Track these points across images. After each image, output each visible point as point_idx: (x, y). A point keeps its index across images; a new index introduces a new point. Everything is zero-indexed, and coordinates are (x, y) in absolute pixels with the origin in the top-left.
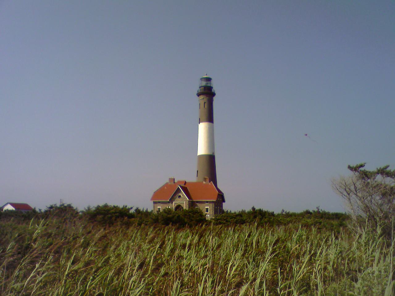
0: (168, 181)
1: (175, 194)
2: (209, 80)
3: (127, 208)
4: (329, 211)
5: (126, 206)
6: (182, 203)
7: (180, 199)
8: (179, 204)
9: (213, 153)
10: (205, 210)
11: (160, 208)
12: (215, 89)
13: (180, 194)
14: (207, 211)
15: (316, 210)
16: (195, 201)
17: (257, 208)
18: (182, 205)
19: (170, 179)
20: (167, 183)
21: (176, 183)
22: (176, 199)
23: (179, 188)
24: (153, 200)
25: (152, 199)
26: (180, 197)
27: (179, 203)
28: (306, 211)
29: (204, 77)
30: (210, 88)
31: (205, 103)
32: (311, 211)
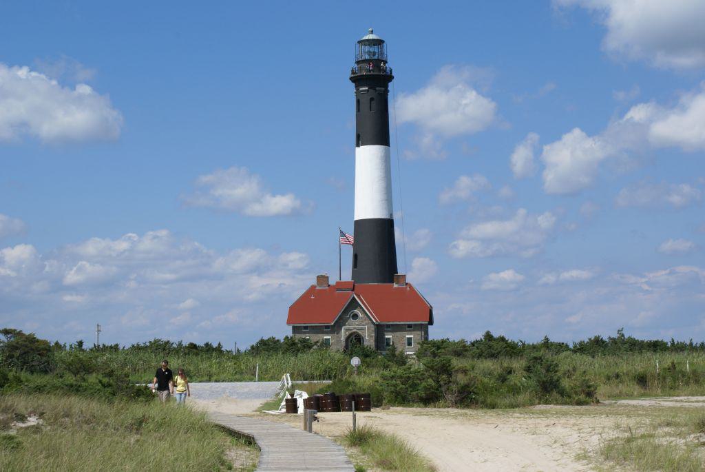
0: (314, 282)
1: (346, 311)
2: (379, 43)
3: (592, 339)
4: (158, 337)
5: (34, 335)
6: (361, 329)
7: (356, 322)
8: (355, 330)
9: (391, 215)
10: (406, 342)
11: (411, 338)
12: (394, 63)
13: (357, 311)
14: (410, 344)
15: (615, 336)
16: (384, 325)
17: (496, 334)
18: (360, 332)
19: (318, 277)
20: (313, 287)
21: (334, 287)
22: (349, 321)
23: (354, 298)
24: (292, 323)
25: (288, 323)
26: (355, 316)
27: (354, 328)
28: (596, 337)
29: (367, 38)
30: (378, 62)
31: (372, 99)
32: (606, 339)
